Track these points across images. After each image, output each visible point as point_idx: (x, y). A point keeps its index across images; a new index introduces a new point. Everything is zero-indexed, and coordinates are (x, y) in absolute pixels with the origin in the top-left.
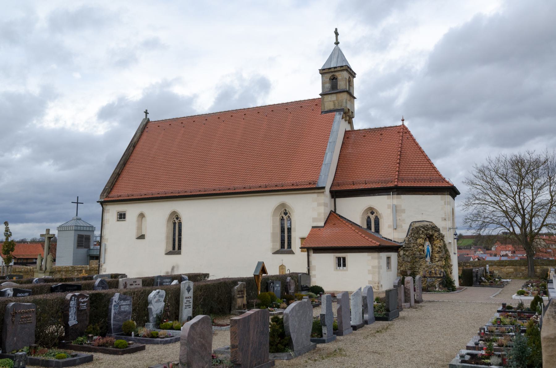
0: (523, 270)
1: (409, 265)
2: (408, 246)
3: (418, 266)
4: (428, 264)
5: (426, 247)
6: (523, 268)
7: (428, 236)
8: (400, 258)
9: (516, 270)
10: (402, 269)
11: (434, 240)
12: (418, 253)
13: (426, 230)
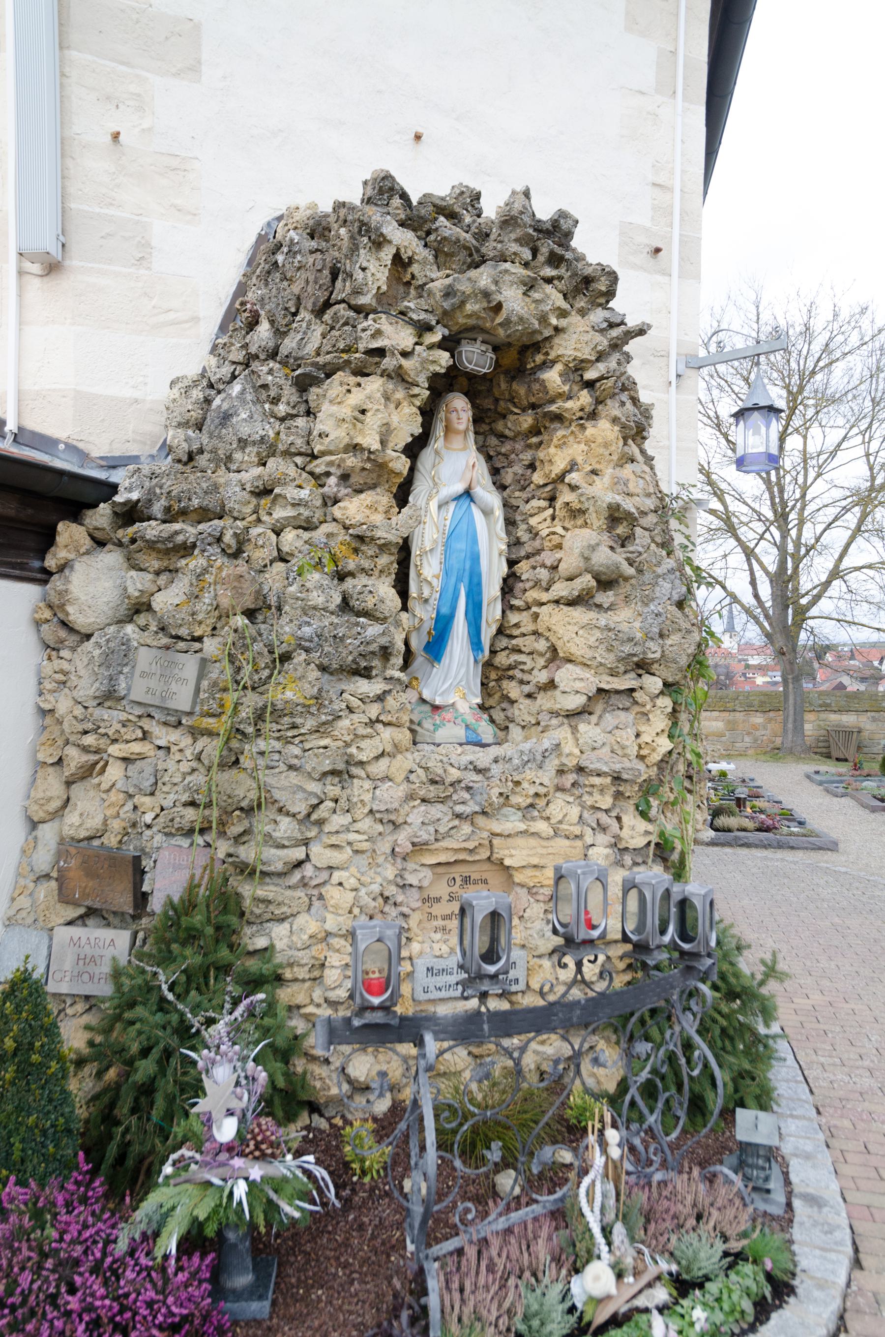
0: (755, 727)
1: (180, 763)
2: (193, 487)
3: (292, 790)
4: (450, 745)
5: (430, 521)
6: (758, 719)
7: (476, 358)
8: (82, 663)
9: (732, 726)
10: (88, 812)
11: (548, 421)
12: (320, 590)
13: (442, 253)
